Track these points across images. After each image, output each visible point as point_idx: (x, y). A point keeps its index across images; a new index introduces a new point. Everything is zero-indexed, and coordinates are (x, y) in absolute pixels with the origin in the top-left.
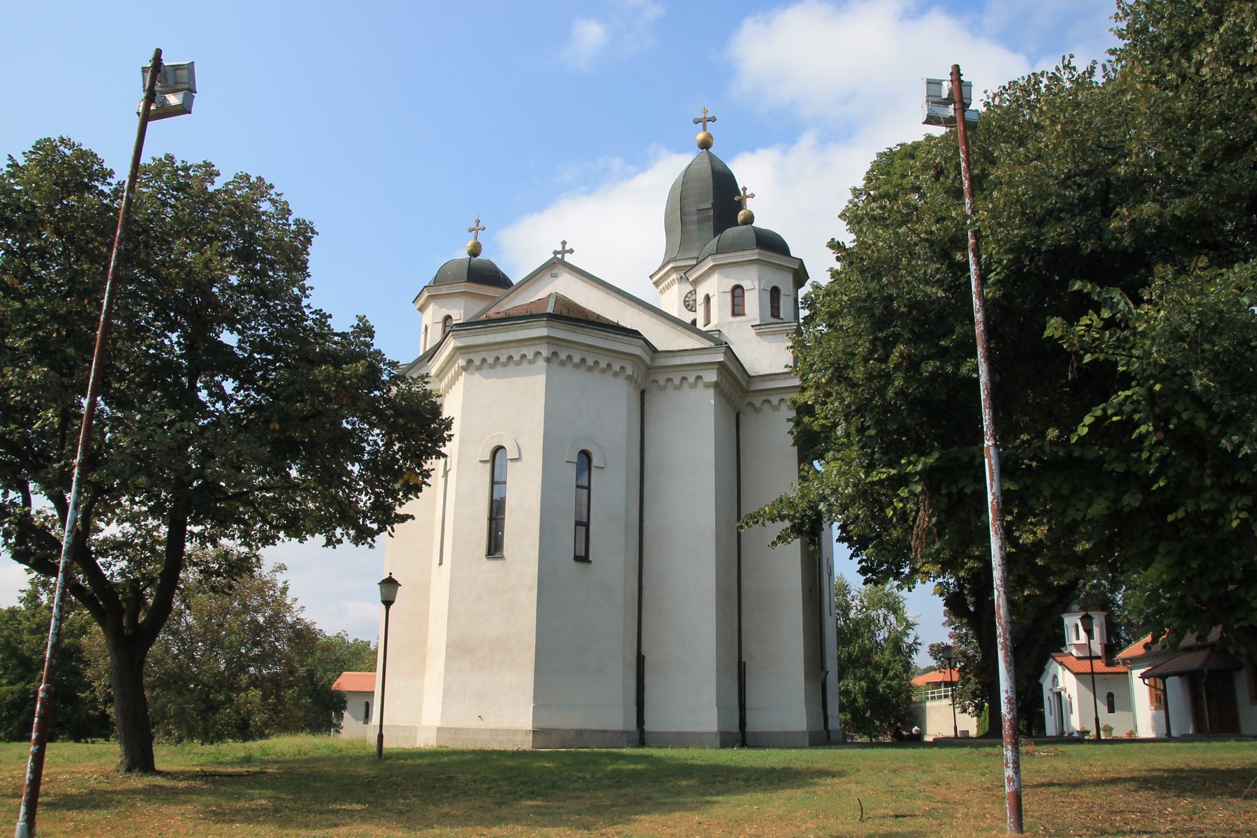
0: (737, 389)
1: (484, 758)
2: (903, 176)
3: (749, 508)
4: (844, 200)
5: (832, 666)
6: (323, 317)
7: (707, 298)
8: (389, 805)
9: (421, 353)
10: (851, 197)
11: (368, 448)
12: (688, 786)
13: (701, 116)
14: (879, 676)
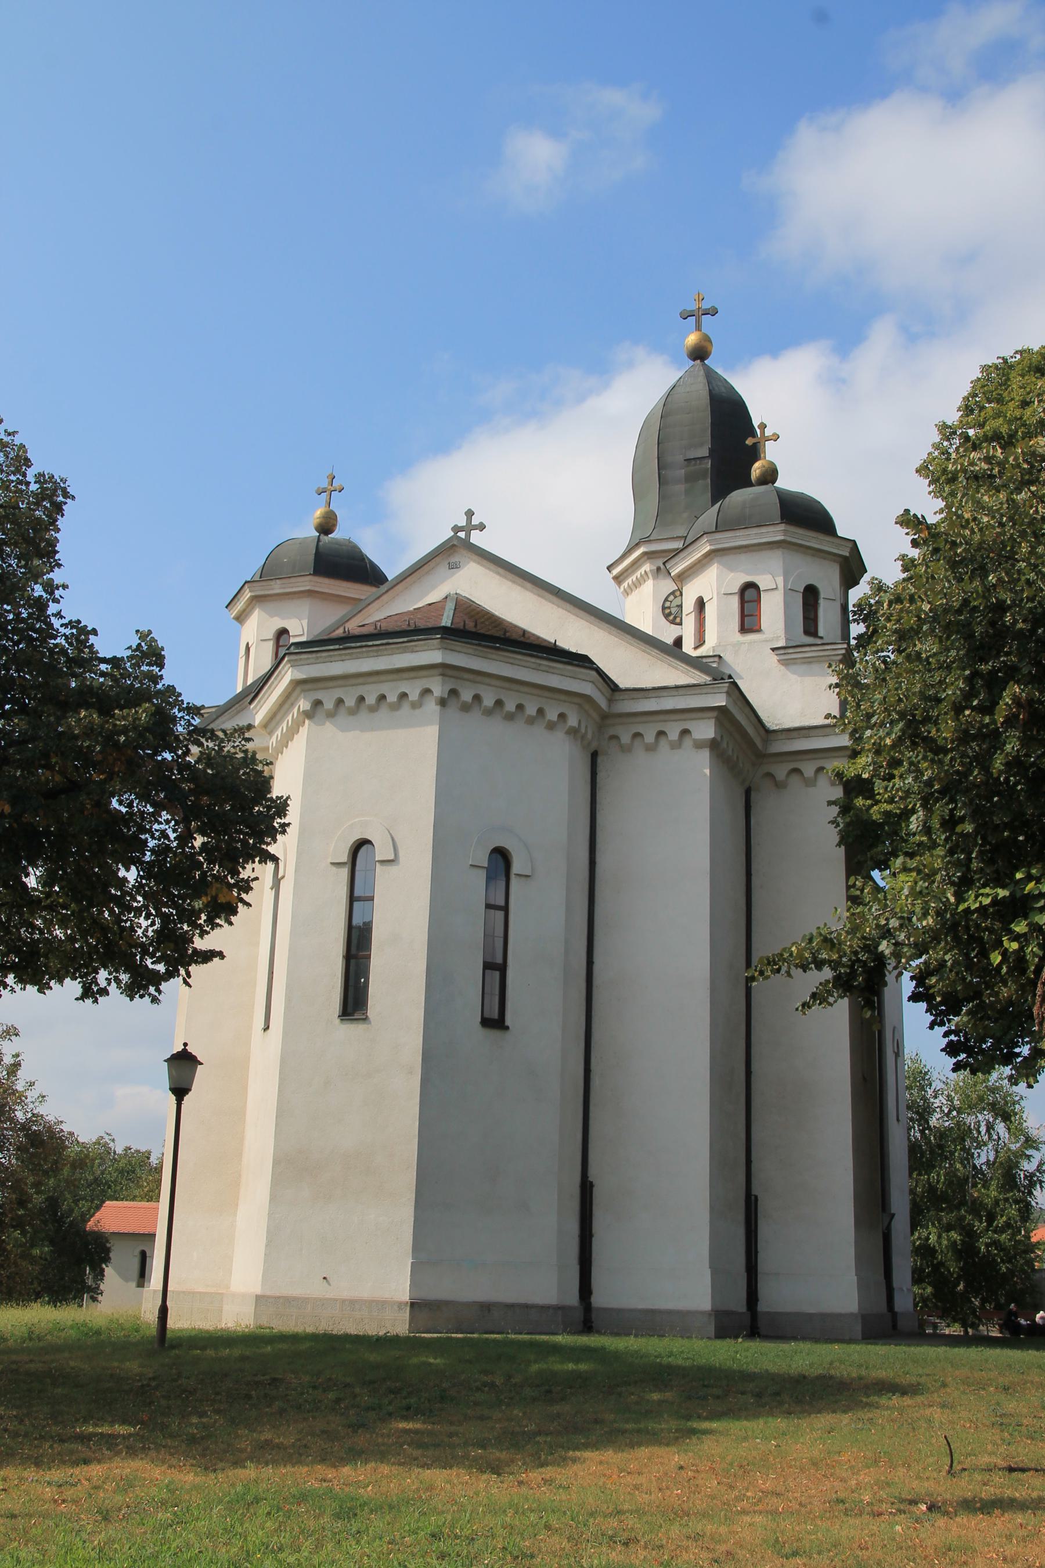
0: (747, 752)
1: (330, 1344)
2: (1025, 404)
3: (762, 949)
4: (924, 442)
5: (900, 1204)
6: (82, 633)
7: (701, 604)
8: (174, 1427)
9: (239, 689)
10: (937, 438)
11: (152, 843)
12: (660, 1402)
13: (693, 306)
14: (979, 1226)
